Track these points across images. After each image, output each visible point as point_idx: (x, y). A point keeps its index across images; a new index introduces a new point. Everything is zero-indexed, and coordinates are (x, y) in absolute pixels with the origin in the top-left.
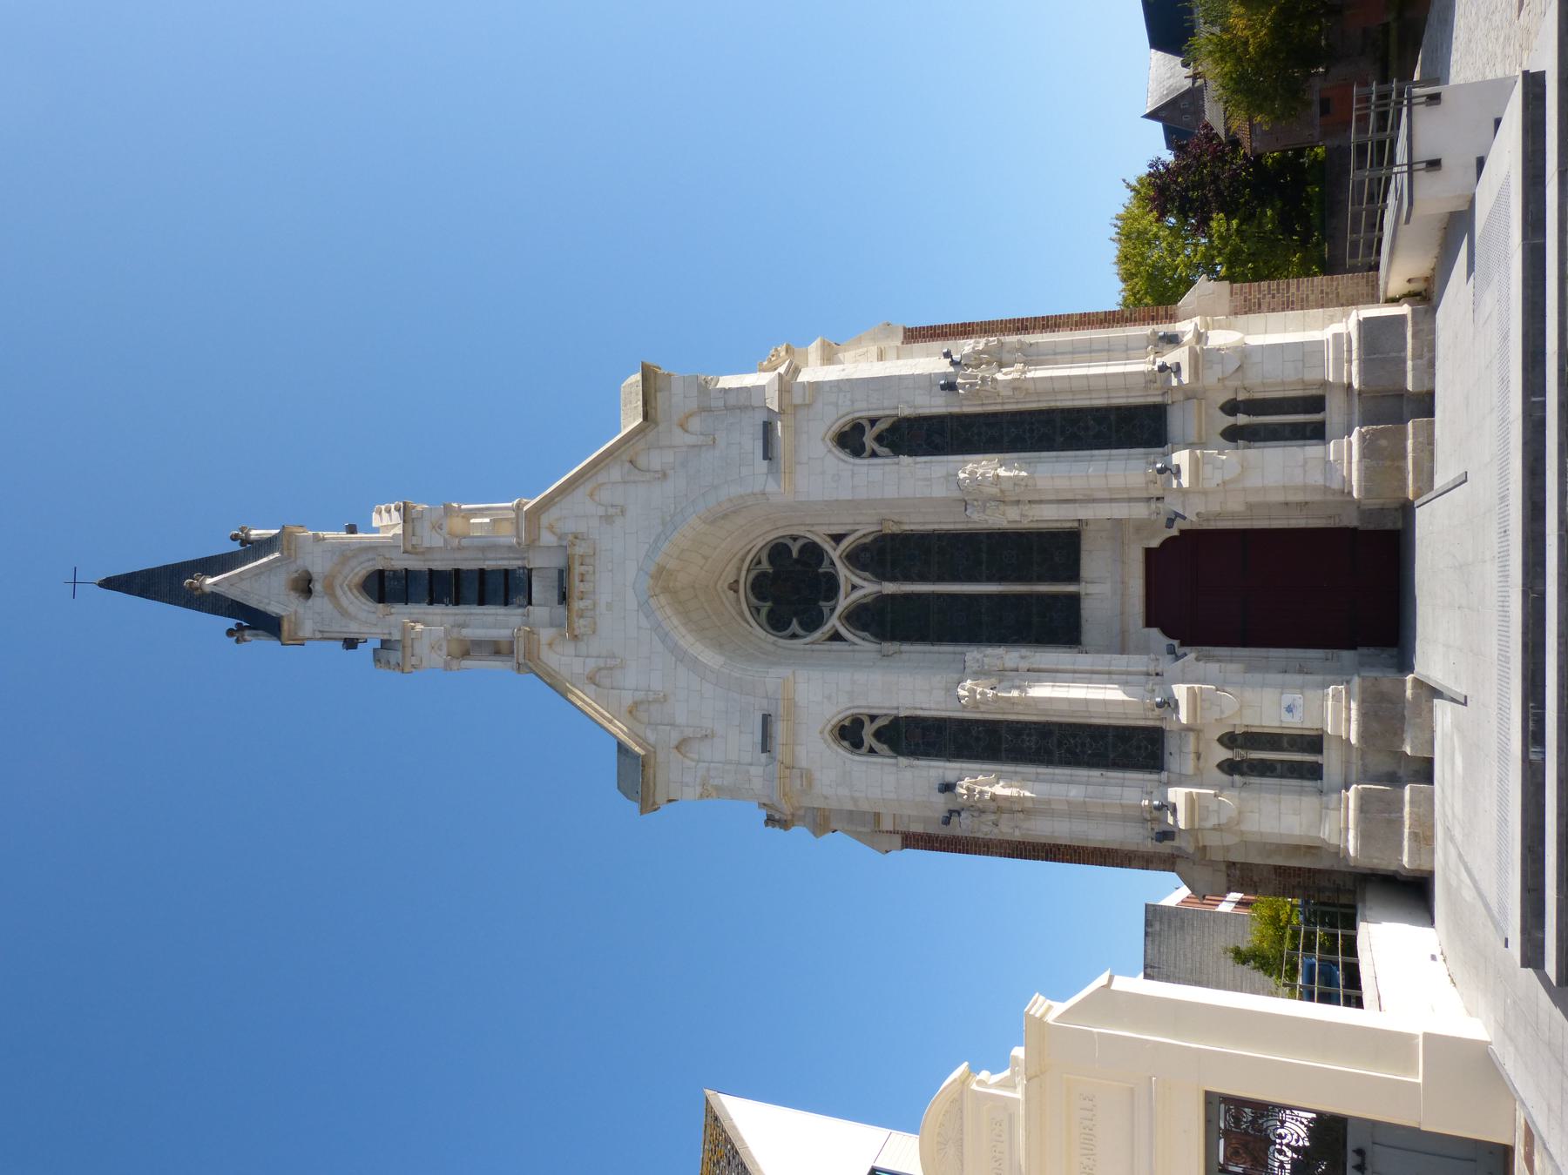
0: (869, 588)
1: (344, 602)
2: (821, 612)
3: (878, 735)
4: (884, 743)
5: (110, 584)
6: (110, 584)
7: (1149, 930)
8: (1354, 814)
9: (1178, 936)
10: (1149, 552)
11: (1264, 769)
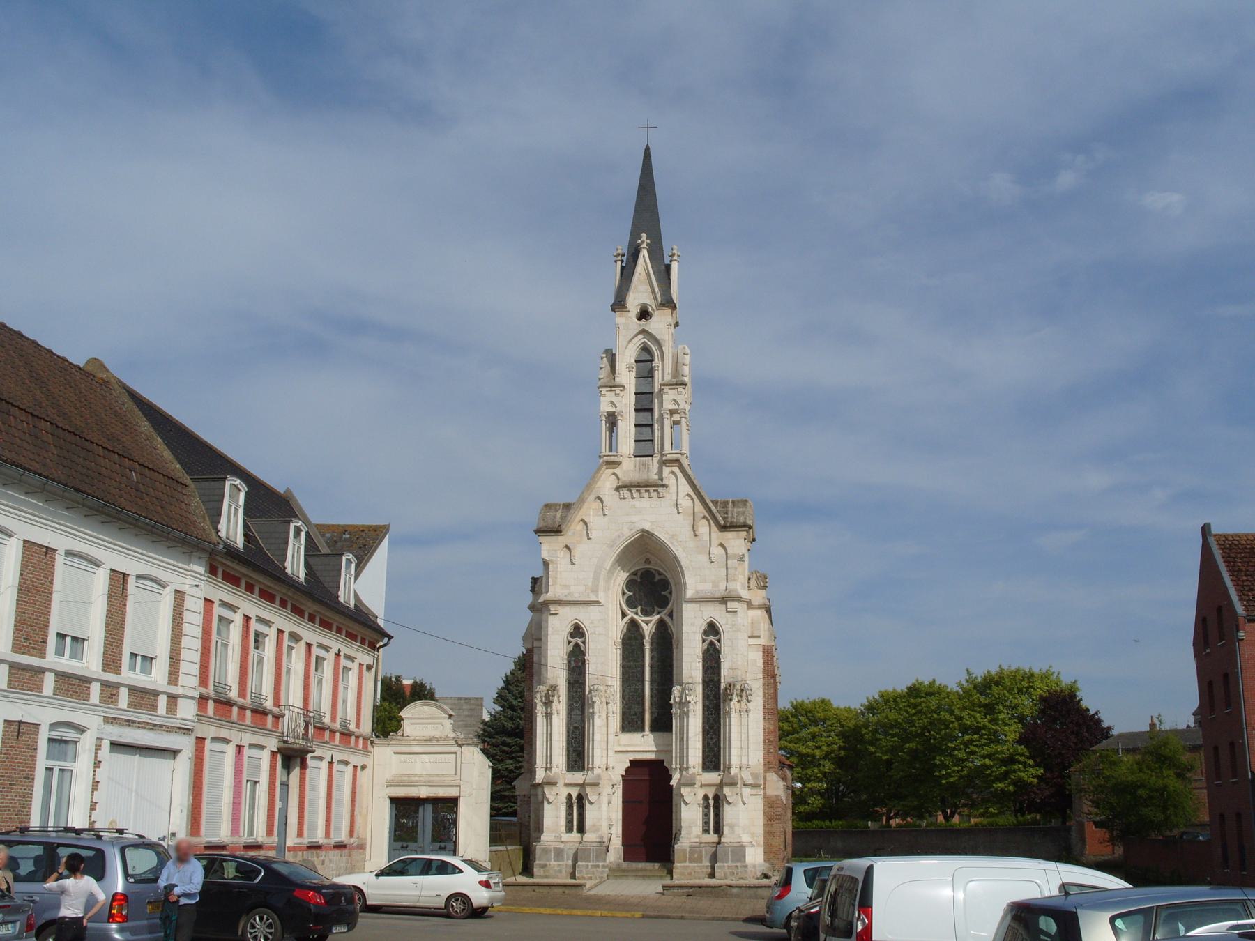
2: (635, 607)
3: (577, 645)
5: (647, 149)
6: (647, 149)
8: (776, 933)
9: (460, 723)
10: (663, 761)
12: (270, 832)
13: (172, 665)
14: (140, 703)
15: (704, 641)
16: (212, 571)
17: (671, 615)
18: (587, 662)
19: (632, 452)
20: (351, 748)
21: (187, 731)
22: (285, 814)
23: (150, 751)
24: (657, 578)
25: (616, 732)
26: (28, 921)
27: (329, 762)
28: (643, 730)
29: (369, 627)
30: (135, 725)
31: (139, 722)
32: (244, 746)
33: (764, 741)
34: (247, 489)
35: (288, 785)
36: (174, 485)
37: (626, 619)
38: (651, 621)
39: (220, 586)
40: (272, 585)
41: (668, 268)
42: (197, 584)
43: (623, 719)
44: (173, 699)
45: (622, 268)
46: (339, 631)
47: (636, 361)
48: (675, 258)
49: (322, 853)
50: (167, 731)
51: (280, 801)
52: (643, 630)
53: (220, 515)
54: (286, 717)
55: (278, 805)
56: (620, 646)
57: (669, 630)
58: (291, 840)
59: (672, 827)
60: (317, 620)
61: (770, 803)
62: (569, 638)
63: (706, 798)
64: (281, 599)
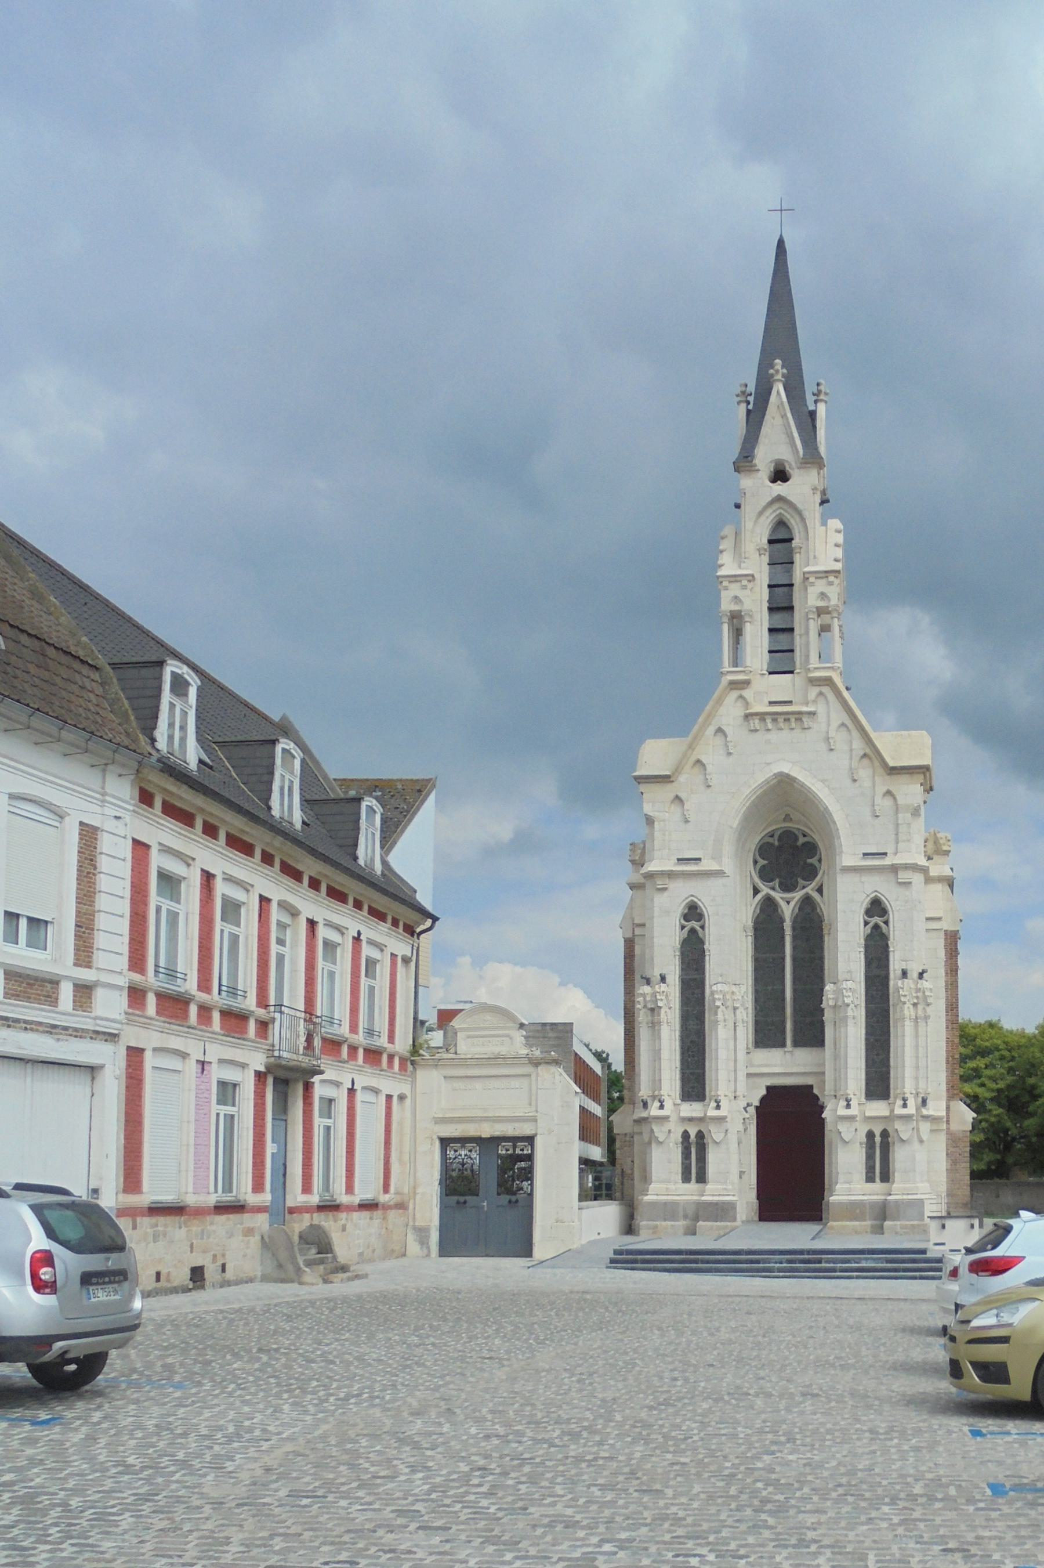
0: (788, 912)
1: (769, 511)
3: (693, 931)
4: (688, 935)
5: (781, 244)
6: (781, 244)
7: (548, 1027)
10: (811, 1087)
11: (686, 1155)
12: (258, 1186)
13: (80, 937)
14: (25, 992)
15: (866, 923)
16: (146, 798)
17: (820, 890)
18: (707, 953)
19: (765, 667)
20: (381, 1070)
21: (112, 1037)
22: (282, 1162)
23: (51, 1066)
24: (802, 840)
25: (747, 1048)
26: (190, 1290)
27: (348, 1089)
28: (783, 1045)
29: (403, 901)
30: (18, 1025)
31: (26, 1022)
32: (210, 1063)
33: (947, 1058)
34: (199, 683)
35: (286, 1120)
36: (77, 665)
37: (759, 896)
38: (793, 898)
39: (158, 823)
40: (247, 829)
41: (813, 415)
42: (118, 815)
43: (756, 1031)
44: (84, 992)
45: (749, 412)
46: (358, 905)
47: (770, 542)
48: (822, 397)
49: (343, 1215)
50: (76, 1037)
51: (273, 1142)
52: (782, 911)
53: (156, 717)
54: (277, 1024)
55: (270, 1148)
56: (751, 933)
57: (818, 910)
58: (296, 1197)
59: (824, 1174)
60: (324, 888)
61: (953, 1140)
62: (683, 922)
63: (870, 1135)
64: (264, 852)
